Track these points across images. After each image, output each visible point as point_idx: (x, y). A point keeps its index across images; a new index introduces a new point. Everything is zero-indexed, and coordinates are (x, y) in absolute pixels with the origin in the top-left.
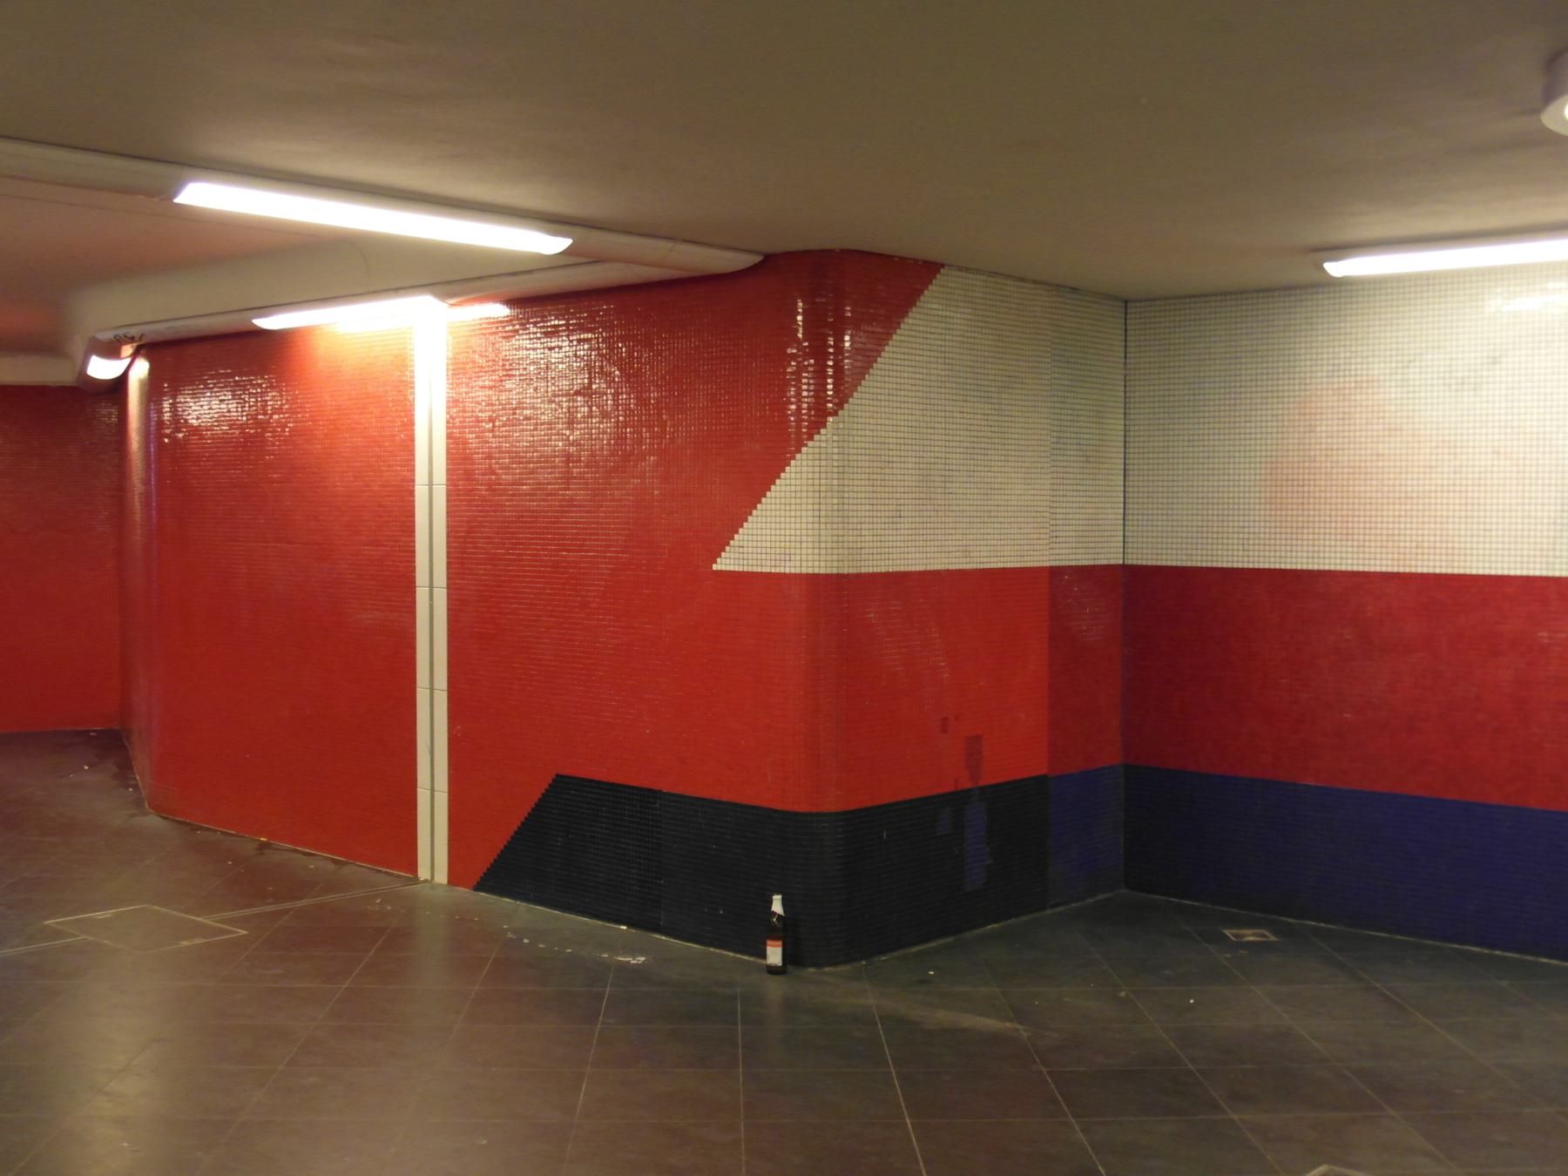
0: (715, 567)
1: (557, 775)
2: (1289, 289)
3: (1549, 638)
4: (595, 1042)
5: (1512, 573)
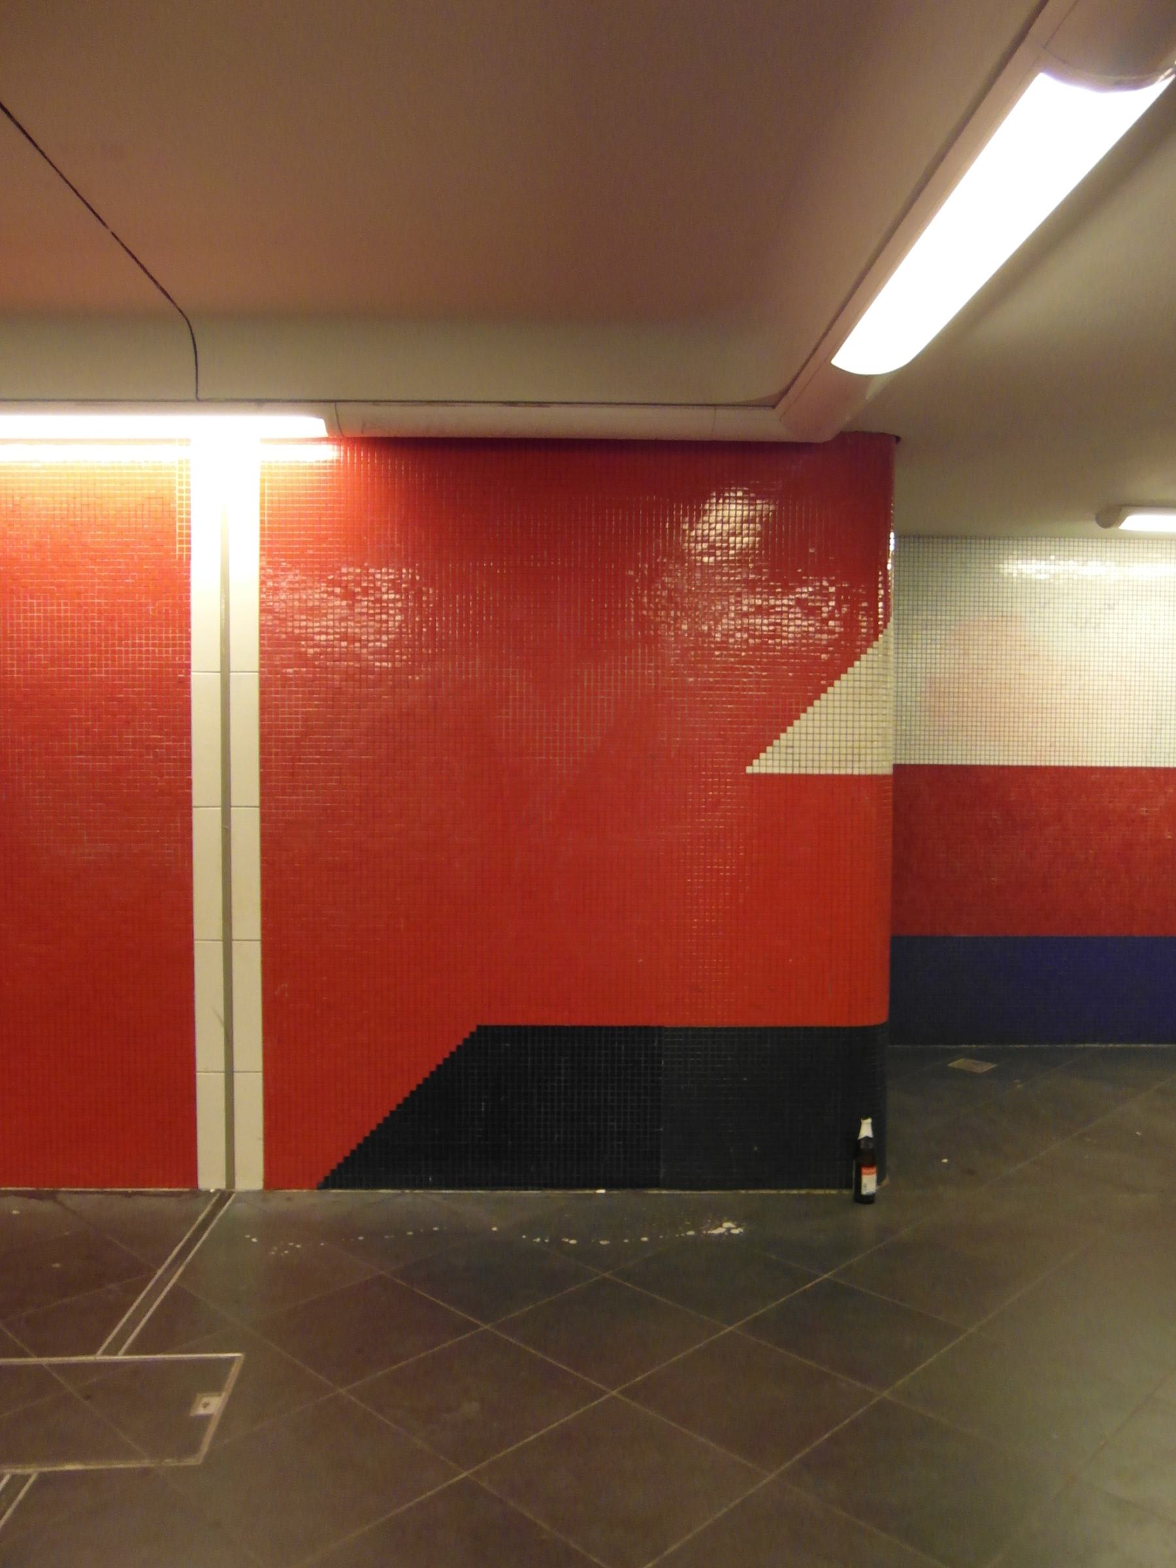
0: (749, 770)
1: (479, 1027)
2: (948, 537)
3: (1147, 811)
4: (961, 1338)
5: (1121, 765)
